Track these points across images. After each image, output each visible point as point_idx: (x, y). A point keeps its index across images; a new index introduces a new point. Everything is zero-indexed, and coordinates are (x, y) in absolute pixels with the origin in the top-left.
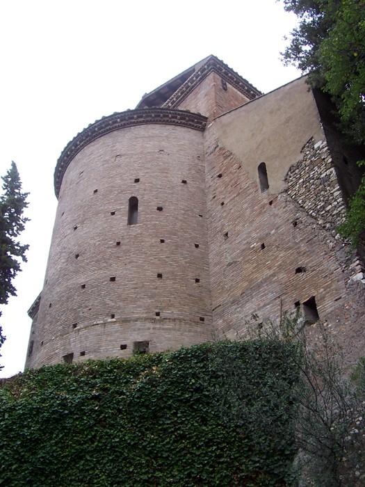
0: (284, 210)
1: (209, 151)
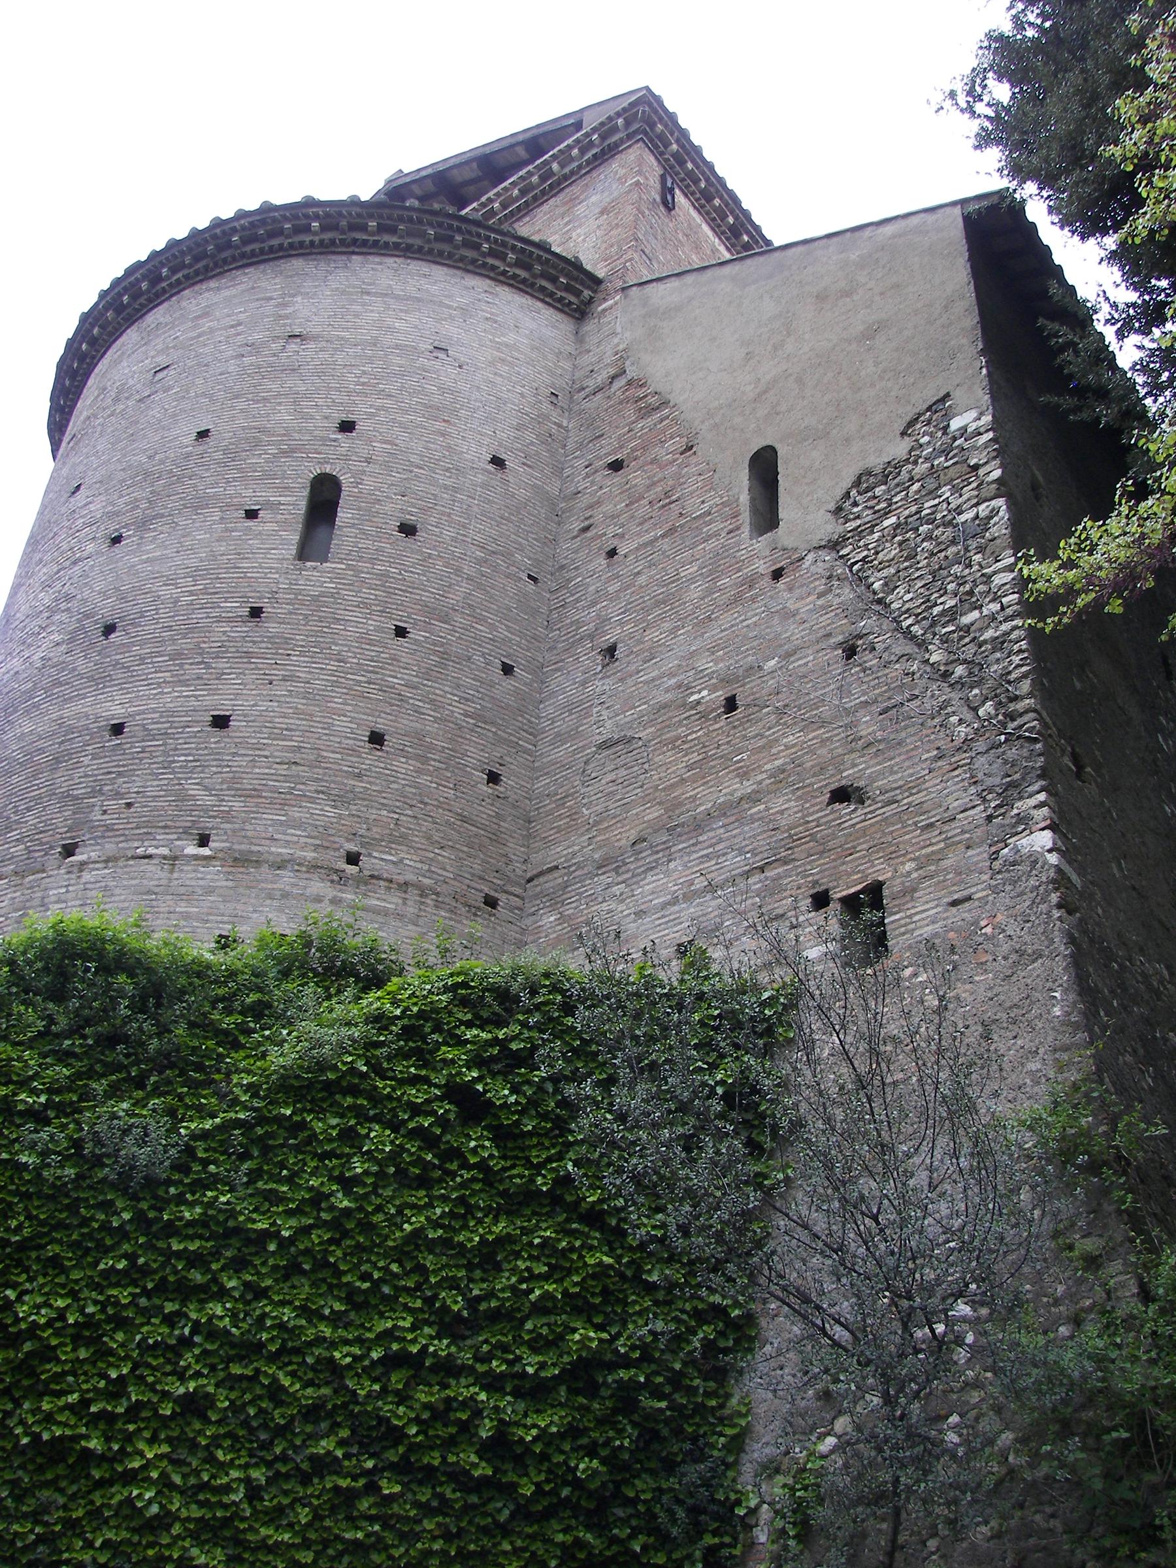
0: (820, 602)
1: (591, 384)
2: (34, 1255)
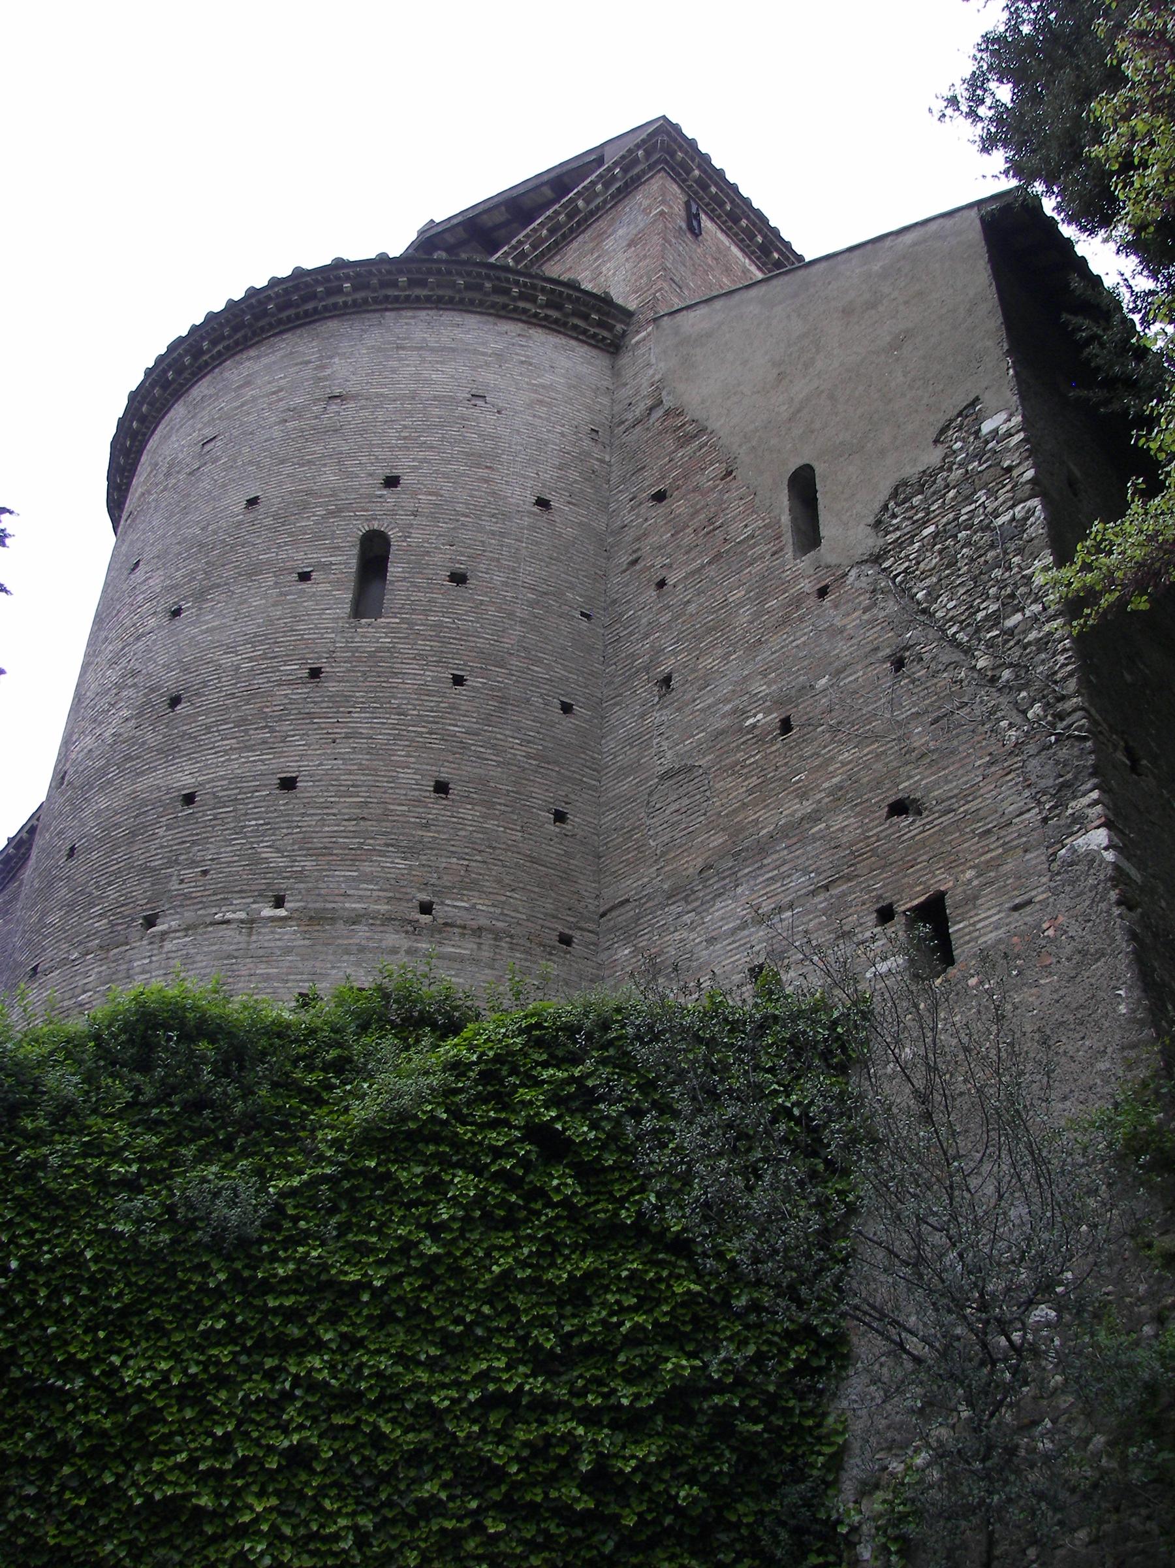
0: (865, 617)
1: (630, 416)
2: (135, 1320)
